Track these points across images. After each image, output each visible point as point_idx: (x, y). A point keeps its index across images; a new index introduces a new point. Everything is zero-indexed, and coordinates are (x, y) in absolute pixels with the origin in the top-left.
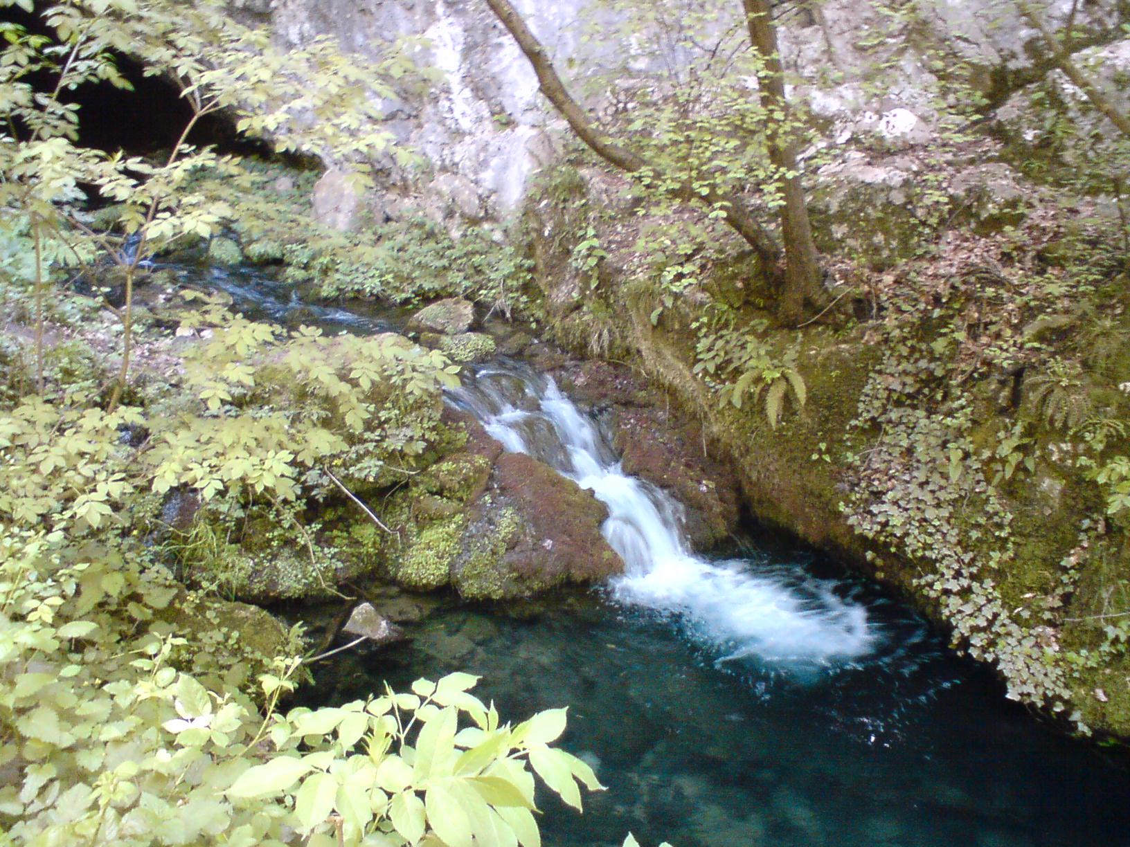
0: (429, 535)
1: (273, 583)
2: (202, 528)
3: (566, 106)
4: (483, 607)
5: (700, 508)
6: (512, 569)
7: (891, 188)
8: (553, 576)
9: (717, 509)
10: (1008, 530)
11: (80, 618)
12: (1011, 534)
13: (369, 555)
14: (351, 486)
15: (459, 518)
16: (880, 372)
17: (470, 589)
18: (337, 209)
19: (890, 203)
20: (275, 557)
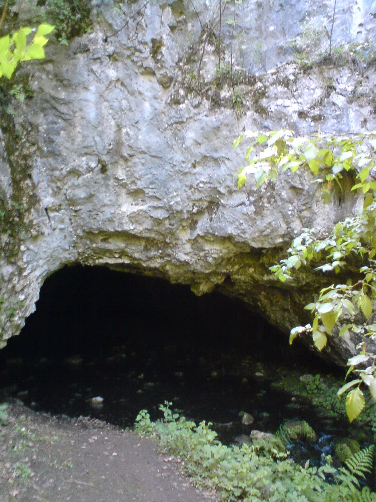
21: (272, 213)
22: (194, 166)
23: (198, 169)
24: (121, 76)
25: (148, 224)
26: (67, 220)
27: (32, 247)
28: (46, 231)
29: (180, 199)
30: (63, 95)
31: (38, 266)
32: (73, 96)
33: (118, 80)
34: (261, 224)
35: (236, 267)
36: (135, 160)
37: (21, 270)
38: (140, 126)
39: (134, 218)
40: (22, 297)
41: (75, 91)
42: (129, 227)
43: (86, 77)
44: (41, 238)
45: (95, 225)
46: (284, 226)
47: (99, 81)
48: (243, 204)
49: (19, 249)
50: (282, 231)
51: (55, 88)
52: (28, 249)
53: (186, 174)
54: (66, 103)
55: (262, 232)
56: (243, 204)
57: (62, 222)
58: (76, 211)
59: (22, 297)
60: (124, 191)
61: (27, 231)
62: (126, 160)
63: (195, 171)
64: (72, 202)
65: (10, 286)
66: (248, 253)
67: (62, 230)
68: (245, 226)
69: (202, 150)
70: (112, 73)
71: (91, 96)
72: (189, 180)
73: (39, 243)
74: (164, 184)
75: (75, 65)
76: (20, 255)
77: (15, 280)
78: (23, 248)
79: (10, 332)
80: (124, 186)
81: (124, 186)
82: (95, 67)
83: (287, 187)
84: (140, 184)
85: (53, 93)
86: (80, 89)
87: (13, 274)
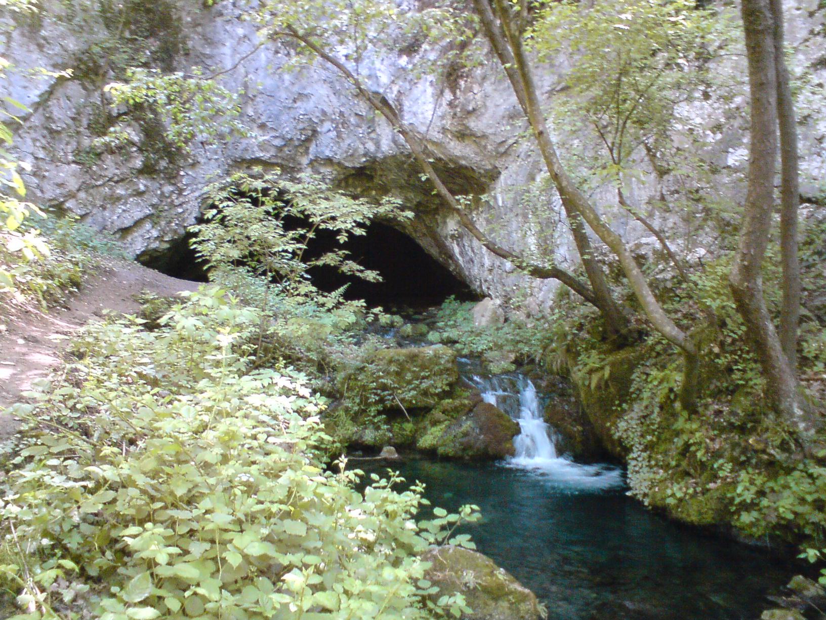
0: (434, 429)
1: (361, 437)
2: (342, 413)
3: (474, 231)
4: (446, 459)
5: (571, 438)
6: (461, 444)
7: (667, 280)
8: (478, 450)
9: (578, 439)
10: (656, 426)
11: (22, 178)
12: (658, 428)
13: (408, 436)
14: (405, 404)
15: (447, 423)
16: (643, 365)
17: (441, 450)
18: (483, 316)
19: (666, 287)
20: (366, 428)
21: (349, 137)
22: (295, 101)
23: (299, 104)
24: (247, 33)
25: (273, 152)
26: (220, 152)
27: (190, 173)
28: (202, 161)
29: (288, 129)
30: (208, 51)
31: (197, 189)
32: (216, 51)
33: (245, 36)
34: (344, 145)
35: (359, 190)
36: (258, 99)
37: (180, 192)
38: (259, 72)
39: (262, 147)
40: (180, 210)
41: (216, 47)
42: (260, 154)
43: (222, 36)
44: (198, 166)
45: (238, 154)
46: (361, 146)
47: (232, 38)
48: (330, 130)
49: (178, 173)
50: (361, 151)
51: (203, 46)
52: (188, 174)
53: (289, 108)
54: (210, 57)
55: (347, 152)
56: (330, 130)
57: (216, 154)
58: (225, 144)
59: (180, 210)
60: (255, 125)
61: (186, 160)
62: (252, 100)
63: (295, 105)
64: (221, 136)
65: (169, 200)
66: (353, 174)
67: (216, 159)
68: (335, 148)
69: (296, 89)
70: (240, 31)
71: (227, 50)
72: (293, 113)
73: (197, 170)
74: (277, 117)
75: (215, 26)
76: (179, 178)
77: (174, 196)
78: (182, 173)
79: (170, 235)
80: (254, 121)
81: (254, 121)
82: (228, 28)
83: (353, 115)
84: (264, 119)
85: (200, 49)
86: (220, 46)
87: (173, 192)
